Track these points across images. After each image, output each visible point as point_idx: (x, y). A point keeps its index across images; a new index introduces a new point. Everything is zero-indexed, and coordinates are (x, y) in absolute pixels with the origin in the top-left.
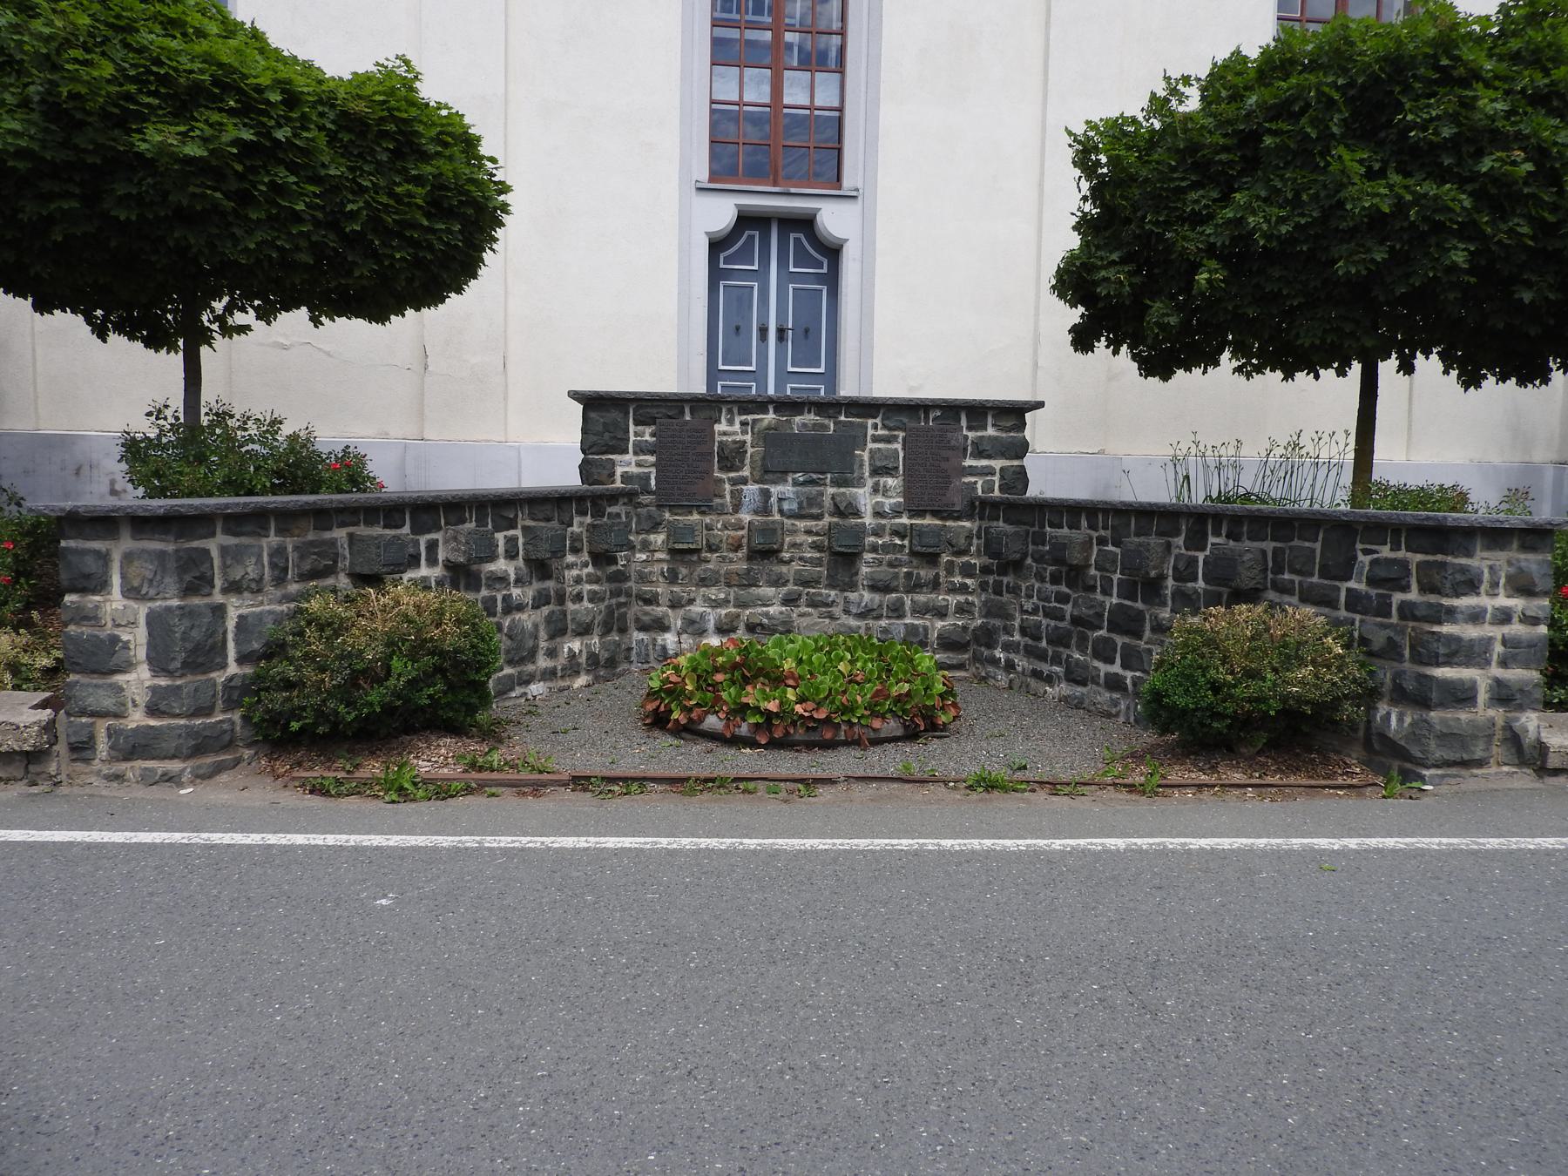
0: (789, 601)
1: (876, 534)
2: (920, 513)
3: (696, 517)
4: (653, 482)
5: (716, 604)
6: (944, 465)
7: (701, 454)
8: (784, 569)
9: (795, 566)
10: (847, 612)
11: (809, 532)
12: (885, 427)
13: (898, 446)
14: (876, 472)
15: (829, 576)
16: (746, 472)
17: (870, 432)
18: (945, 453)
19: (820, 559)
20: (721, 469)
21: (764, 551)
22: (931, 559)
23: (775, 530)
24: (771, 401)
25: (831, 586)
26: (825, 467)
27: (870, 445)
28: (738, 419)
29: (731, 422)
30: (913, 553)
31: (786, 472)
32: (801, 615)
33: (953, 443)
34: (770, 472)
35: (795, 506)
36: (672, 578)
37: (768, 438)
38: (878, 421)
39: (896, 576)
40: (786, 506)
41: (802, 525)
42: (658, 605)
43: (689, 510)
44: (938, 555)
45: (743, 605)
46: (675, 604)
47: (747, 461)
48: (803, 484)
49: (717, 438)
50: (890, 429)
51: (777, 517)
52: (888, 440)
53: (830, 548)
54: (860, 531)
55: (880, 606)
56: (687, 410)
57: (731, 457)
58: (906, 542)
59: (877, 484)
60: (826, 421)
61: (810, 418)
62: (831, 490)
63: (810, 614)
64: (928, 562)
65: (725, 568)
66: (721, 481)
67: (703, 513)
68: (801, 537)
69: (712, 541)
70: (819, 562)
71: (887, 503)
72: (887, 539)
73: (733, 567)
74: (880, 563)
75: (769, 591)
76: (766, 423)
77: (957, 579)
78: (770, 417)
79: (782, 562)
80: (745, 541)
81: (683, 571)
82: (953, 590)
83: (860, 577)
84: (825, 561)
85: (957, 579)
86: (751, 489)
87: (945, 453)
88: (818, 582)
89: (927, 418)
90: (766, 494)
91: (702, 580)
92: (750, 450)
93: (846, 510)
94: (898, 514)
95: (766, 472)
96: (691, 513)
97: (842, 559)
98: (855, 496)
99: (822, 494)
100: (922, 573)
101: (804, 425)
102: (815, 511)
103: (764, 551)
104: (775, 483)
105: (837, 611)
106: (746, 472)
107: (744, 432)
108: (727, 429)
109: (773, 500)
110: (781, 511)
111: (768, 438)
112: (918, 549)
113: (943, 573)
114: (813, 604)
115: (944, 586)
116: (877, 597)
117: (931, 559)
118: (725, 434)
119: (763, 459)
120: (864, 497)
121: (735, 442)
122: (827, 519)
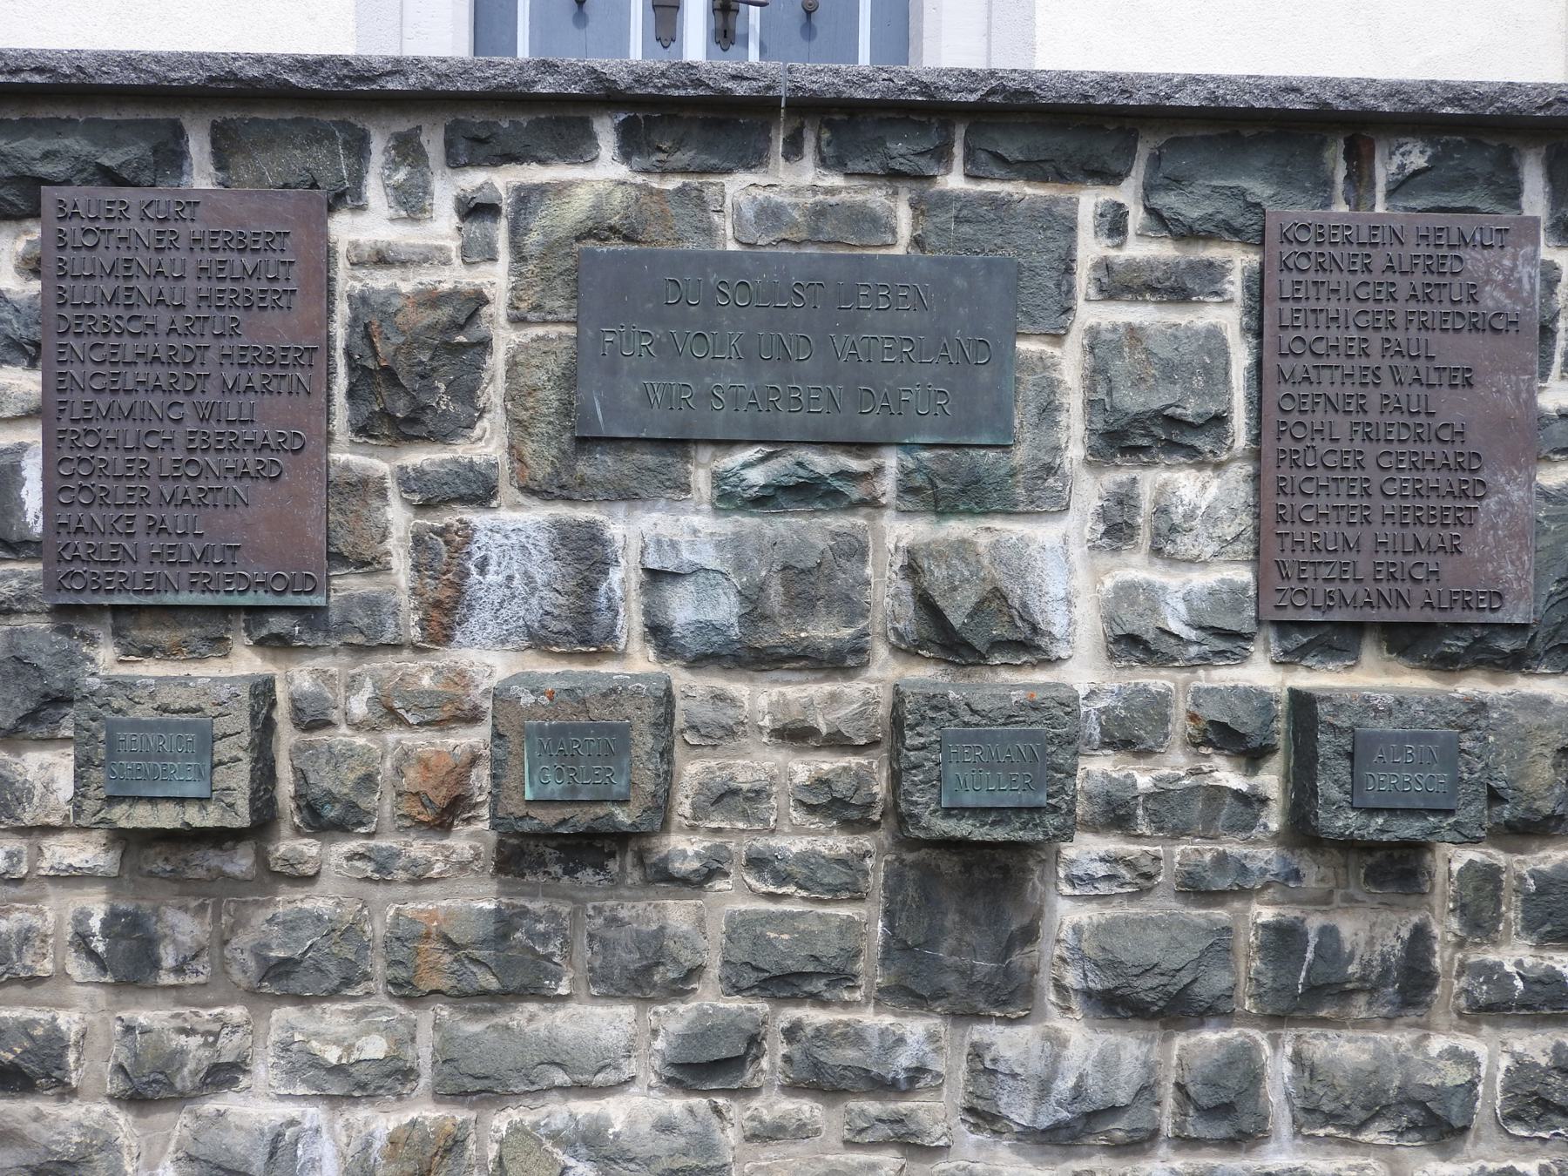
0: (706, 1068)
1: (1124, 739)
2: (1333, 640)
3: (245, 662)
4: (32, 496)
5: (349, 1085)
6: (1450, 406)
7: (274, 360)
8: (678, 913)
9: (735, 897)
10: (983, 1117)
11: (795, 735)
12: (1160, 221)
13: (1224, 316)
14: (1119, 440)
15: (896, 948)
16: (486, 445)
17: (1090, 248)
18: (1453, 349)
19: (850, 863)
20: (363, 430)
21: (577, 839)
22: (1396, 868)
23: (615, 739)
24: (607, 97)
25: (908, 994)
26: (869, 424)
27: (1092, 314)
28: (447, 188)
29: (411, 203)
30: (1303, 832)
31: (679, 445)
32: (766, 1134)
33: (1492, 299)
34: (605, 446)
35: (725, 609)
36: (130, 959)
37: (598, 274)
38: (1127, 193)
39: (1220, 944)
40: (683, 608)
41: (760, 697)
42: (66, 1092)
43: (211, 625)
44: (1417, 848)
45: (474, 1087)
46: (146, 1091)
47: (494, 391)
48: (765, 500)
49: (346, 281)
50: (1186, 234)
51: (641, 662)
52: (1174, 289)
53: (900, 818)
54: (1049, 735)
55: (1147, 1091)
56: (198, 147)
57: (414, 375)
58: (1270, 780)
59: (1124, 499)
60: (875, 197)
61: (795, 180)
62: (901, 531)
63: (802, 1131)
64: (1376, 877)
65: (391, 908)
66: (364, 488)
67: (277, 645)
68: (759, 763)
69: (324, 779)
70: (841, 882)
71: (1181, 591)
72: (1175, 764)
73: (429, 905)
74: (1144, 880)
75: (603, 1023)
76: (577, 208)
77: (1515, 955)
78: (600, 177)
79: (663, 877)
80: (481, 777)
81: (183, 927)
82: (1495, 1006)
83: (1047, 951)
84: (876, 872)
85: (1515, 955)
86: (513, 531)
87: (1453, 349)
88: (842, 977)
89: (1360, 178)
90: (585, 554)
91: (278, 970)
92: (505, 339)
93: (972, 630)
94: (1228, 642)
95: (586, 443)
96: (219, 645)
97: (963, 889)
98: (1017, 561)
99: (856, 550)
100: (1351, 928)
101: (770, 214)
102: (825, 631)
103: (577, 839)
104: (626, 495)
105: (934, 1112)
106: (486, 445)
107: (477, 253)
108: (398, 235)
109: (622, 579)
110: (659, 634)
111: (598, 274)
112: (1347, 822)
113: (1445, 927)
114: (817, 1081)
115: (1450, 989)
116: (1131, 1048)
117: (1396, 868)
118: (382, 259)
119: (569, 379)
120: (1061, 565)
121: (432, 299)
122: (886, 672)
